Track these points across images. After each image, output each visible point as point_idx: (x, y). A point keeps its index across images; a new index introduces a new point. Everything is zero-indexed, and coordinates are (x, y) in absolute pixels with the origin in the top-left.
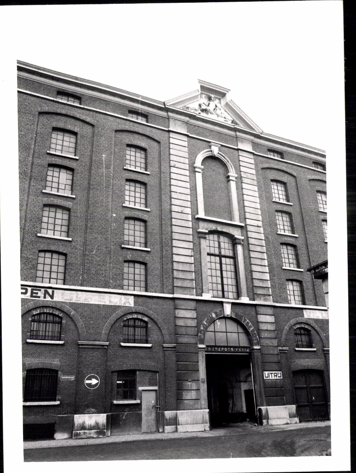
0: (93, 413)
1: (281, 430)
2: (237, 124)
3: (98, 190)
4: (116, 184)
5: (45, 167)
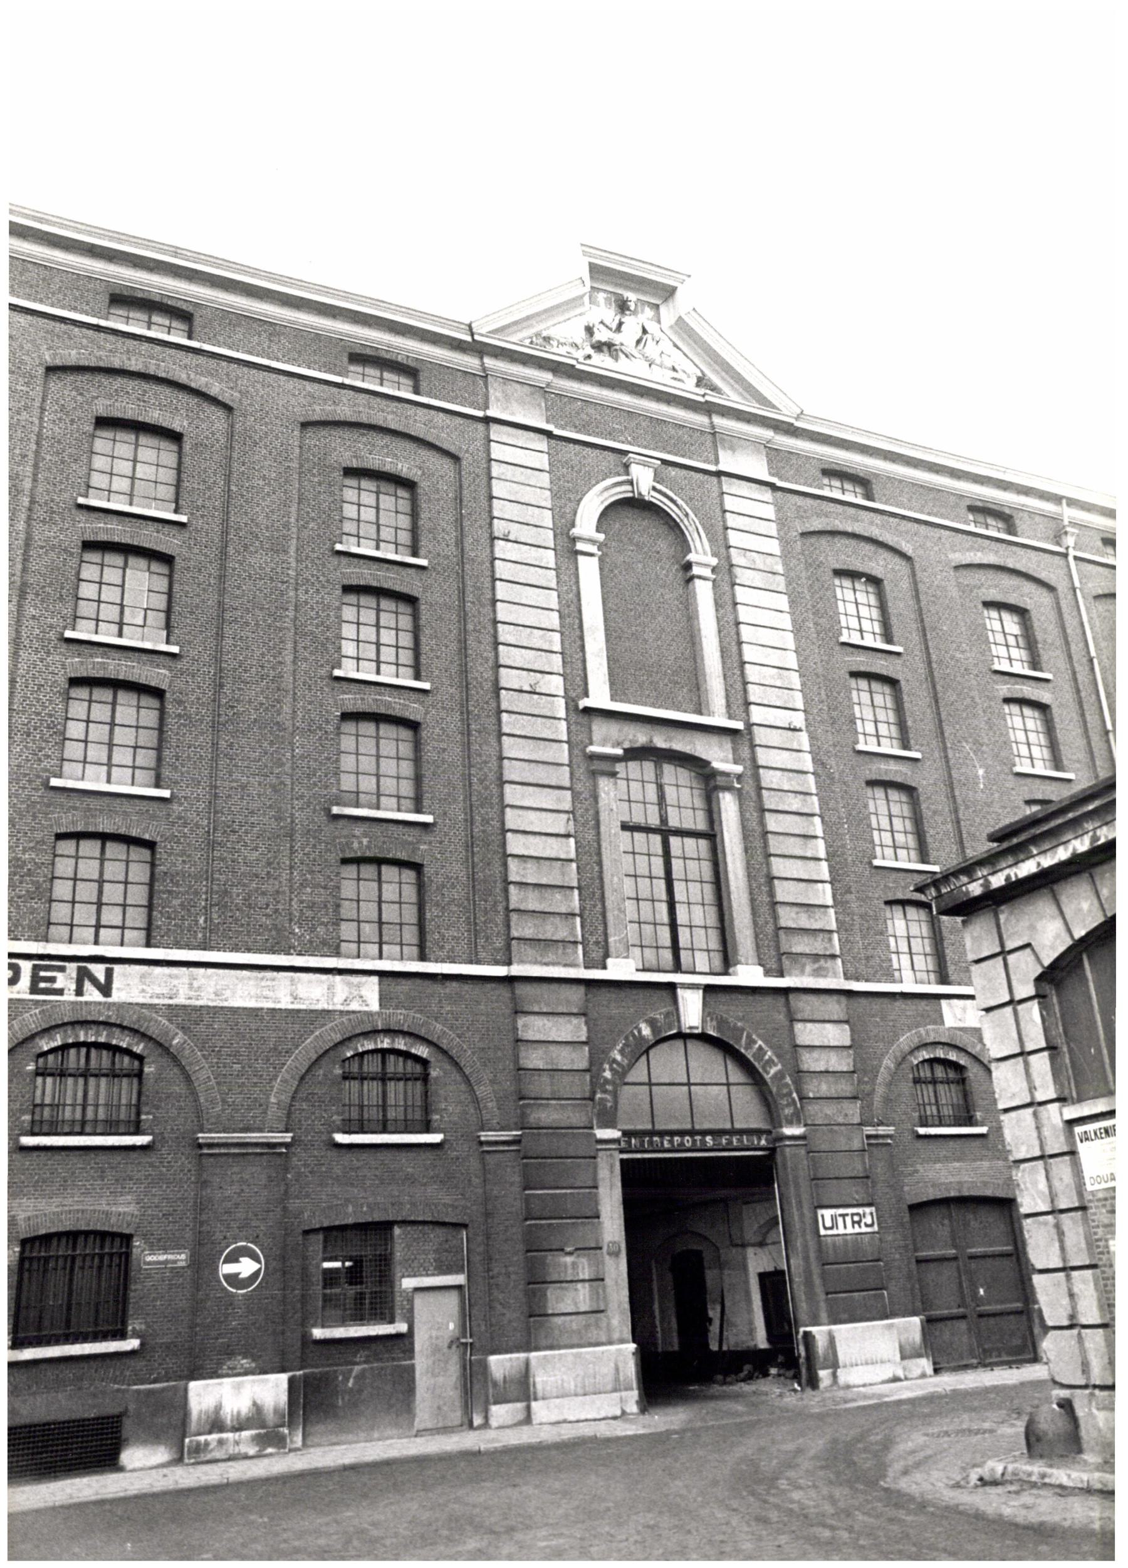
0: (246, 1374)
1: (871, 1402)
2: (714, 388)
3: (247, 624)
4: (306, 603)
5: (72, 554)
